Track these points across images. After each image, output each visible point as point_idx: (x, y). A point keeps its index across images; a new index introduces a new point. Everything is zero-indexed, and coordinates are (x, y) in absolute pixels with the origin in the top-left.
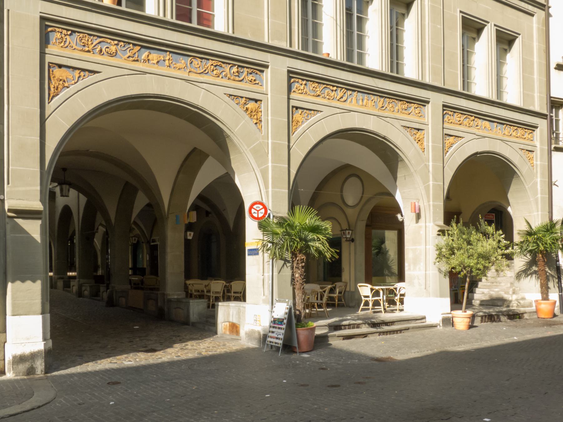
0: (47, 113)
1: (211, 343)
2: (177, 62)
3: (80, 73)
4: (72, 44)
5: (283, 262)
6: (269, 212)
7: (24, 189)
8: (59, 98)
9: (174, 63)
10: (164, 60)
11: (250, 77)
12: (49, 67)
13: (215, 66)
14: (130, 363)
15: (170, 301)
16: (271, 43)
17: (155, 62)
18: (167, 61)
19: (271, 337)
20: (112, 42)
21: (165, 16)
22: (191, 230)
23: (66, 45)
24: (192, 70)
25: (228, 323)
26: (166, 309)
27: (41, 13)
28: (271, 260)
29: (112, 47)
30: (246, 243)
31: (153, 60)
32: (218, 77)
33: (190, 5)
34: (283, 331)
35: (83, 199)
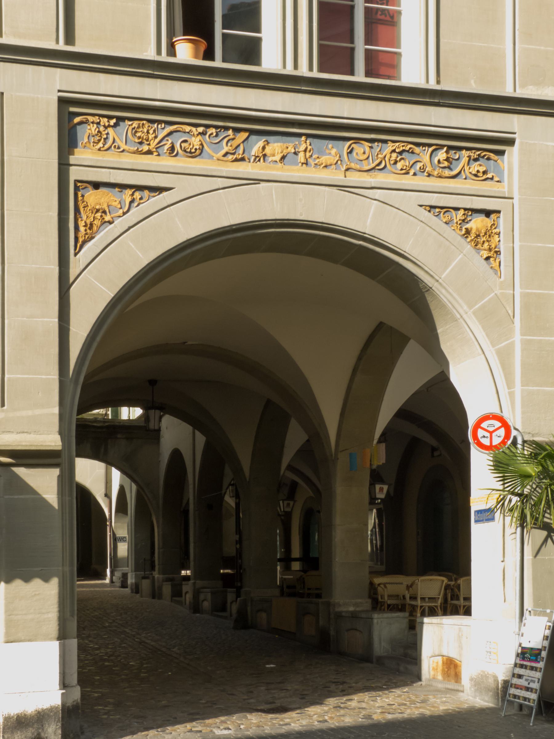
0: (73, 272)
1: (400, 696)
2: (321, 153)
3: (132, 195)
4: (118, 142)
5: (544, 533)
6: (514, 433)
7: (30, 413)
8: (94, 245)
9: (314, 156)
10: (296, 153)
11: (475, 167)
12: (77, 189)
13: (401, 153)
14: (226, 732)
15: (339, 616)
16: (522, 92)
17: (278, 158)
18: (301, 155)
19: (517, 687)
20: (194, 129)
21: (296, 67)
22: (382, 481)
23: (106, 146)
24: (353, 165)
25: (440, 659)
26: (332, 633)
27: (59, 91)
28: (519, 529)
29: (193, 138)
30: (472, 498)
31: (274, 155)
32: (407, 173)
33: (352, 41)
34: (538, 675)
35: (201, 439)
